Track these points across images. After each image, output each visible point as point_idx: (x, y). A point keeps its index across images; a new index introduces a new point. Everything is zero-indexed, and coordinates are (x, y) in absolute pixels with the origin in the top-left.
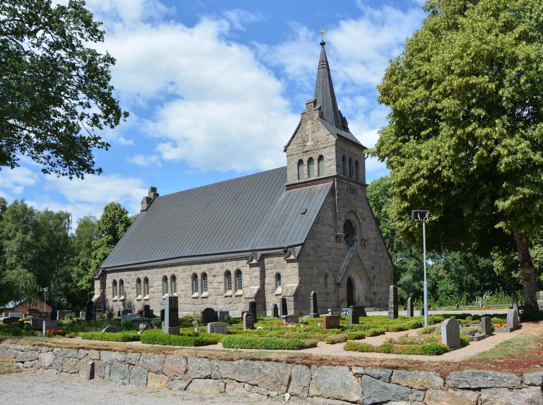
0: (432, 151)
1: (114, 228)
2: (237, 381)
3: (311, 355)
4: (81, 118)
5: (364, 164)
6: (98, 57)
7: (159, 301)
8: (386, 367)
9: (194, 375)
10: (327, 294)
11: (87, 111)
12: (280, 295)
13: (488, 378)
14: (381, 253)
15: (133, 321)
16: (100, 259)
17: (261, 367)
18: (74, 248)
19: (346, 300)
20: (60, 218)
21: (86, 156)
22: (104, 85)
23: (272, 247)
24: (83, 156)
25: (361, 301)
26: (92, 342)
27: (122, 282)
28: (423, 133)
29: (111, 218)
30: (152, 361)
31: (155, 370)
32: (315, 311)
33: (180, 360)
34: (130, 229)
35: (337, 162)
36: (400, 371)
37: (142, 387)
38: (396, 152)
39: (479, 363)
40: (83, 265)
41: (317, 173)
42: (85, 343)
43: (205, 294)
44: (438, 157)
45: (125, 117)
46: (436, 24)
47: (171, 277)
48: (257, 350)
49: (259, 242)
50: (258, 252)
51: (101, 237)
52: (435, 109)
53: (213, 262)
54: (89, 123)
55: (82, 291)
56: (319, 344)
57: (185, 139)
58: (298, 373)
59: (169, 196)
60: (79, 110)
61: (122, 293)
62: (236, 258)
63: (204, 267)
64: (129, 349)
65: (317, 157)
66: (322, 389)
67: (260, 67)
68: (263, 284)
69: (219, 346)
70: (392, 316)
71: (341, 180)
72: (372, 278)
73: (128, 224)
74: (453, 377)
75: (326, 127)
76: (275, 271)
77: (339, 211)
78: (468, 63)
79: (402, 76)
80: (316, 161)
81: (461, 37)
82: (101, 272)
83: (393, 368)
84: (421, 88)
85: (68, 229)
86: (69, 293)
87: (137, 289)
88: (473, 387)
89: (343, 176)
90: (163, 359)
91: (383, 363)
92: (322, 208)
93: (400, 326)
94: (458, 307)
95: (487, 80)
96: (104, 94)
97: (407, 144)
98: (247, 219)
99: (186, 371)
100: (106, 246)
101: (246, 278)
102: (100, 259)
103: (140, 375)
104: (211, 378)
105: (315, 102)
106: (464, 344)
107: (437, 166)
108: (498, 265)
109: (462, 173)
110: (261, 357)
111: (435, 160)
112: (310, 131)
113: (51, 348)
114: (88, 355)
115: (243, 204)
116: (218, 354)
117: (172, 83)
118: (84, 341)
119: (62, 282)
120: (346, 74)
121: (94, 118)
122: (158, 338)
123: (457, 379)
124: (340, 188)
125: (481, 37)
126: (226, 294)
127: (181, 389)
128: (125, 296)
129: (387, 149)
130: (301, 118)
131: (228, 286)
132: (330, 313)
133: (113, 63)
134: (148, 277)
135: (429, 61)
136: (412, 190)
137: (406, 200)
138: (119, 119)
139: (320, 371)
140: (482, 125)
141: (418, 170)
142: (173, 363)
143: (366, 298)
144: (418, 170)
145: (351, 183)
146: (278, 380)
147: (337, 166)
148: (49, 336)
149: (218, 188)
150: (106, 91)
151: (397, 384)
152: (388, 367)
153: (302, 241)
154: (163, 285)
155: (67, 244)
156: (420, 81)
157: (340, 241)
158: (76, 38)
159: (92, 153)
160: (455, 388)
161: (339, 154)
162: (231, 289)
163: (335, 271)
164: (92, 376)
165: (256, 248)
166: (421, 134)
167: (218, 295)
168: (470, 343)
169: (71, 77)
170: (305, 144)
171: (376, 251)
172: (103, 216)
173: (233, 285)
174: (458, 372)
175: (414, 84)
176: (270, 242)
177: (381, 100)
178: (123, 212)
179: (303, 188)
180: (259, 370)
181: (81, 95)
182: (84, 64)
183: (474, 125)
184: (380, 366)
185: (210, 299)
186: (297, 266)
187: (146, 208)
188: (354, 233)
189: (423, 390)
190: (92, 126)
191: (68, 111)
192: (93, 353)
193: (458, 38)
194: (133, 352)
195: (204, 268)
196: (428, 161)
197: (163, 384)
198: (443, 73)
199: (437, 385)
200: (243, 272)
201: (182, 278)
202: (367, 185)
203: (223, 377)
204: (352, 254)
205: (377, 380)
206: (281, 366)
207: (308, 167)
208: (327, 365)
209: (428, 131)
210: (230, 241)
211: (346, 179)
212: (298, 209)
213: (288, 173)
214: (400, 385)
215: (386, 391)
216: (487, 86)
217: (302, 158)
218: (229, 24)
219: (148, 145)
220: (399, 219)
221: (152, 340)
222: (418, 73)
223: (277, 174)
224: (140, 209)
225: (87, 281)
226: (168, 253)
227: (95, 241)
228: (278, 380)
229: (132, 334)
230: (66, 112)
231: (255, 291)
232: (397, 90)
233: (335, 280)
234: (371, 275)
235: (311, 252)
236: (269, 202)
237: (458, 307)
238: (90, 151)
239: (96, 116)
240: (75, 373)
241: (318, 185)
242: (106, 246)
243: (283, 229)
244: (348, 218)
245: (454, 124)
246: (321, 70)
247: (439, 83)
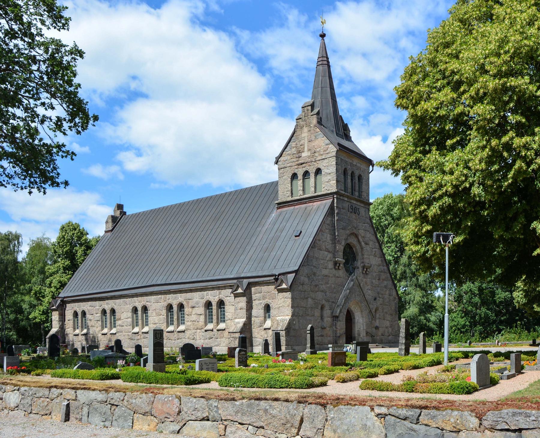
0: (457, 165)
1: (71, 251)
2: (240, 423)
3: (325, 395)
4: (42, 122)
5: (369, 179)
6: (63, 48)
7: (128, 335)
8: (413, 407)
9: (188, 416)
10: (323, 328)
11: (49, 113)
12: (269, 329)
13: (531, 418)
14: (385, 282)
15: (106, 357)
16: (55, 287)
17: (268, 407)
18: (25, 274)
19: (345, 335)
20: (8, 239)
21: (50, 167)
22: (70, 83)
23: (260, 274)
24: (46, 166)
25: (361, 336)
26: (64, 380)
27: (84, 313)
28: (449, 142)
29: (68, 240)
30: (138, 401)
31: (143, 411)
32: (312, 346)
33: (172, 400)
34: (93, 254)
35: (338, 176)
36: (430, 411)
37: (127, 430)
38: (416, 164)
39: (515, 402)
40: (35, 294)
41: (313, 189)
42: (57, 381)
43: (182, 328)
44: (465, 172)
45: (94, 122)
46: (465, 13)
47: (142, 308)
48: (260, 389)
49: (246, 269)
50: (245, 280)
51: (55, 262)
52: (462, 114)
53: (191, 291)
54: (51, 127)
55: (36, 324)
56: (330, 382)
57: (151, 147)
58: (311, 414)
59: (138, 215)
60: (41, 111)
61: (85, 325)
62: (219, 287)
63: (181, 297)
64: (110, 388)
65: (314, 171)
66: (339, 431)
67: (240, 59)
68: (249, 317)
69: (214, 385)
70: (403, 353)
71: (341, 198)
72: (374, 310)
73: (88, 247)
74: (490, 418)
75: (325, 135)
76: (264, 302)
77: (338, 233)
78: (506, 62)
79: (424, 75)
80: (312, 176)
81: (498, 30)
82: (59, 301)
83: (421, 408)
84: (447, 90)
85: (18, 252)
86: (18, 326)
87: (102, 322)
88: (513, 428)
89: (343, 192)
90: (152, 399)
91: (410, 403)
92: (320, 230)
93: (415, 363)
94: (470, 343)
95: (528, 81)
96: (70, 93)
97: (428, 156)
98: (231, 242)
99: (180, 412)
100: (63, 273)
101: (229, 310)
102: (55, 287)
103: (125, 417)
104: (208, 420)
105: (312, 106)
106: (493, 383)
107: (463, 182)
108: (519, 296)
109: (495, 189)
110: (268, 397)
111: (461, 175)
112: (306, 139)
113: (17, 387)
114: (61, 394)
115: (227, 225)
116: (216, 393)
117: (134, 78)
118: (55, 379)
119: (11, 313)
120: (343, 68)
121: (57, 121)
122: (142, 376)
123: (495, 419)
124: (340, 206)
125: (521, 30)
126: (206, 328)
127: (173, 432)
128: (88, 329)
129: (404, 161)
130: (295, 124)
131: (209, 319)
132: (331, 349)
133: (81, 56)
134: (115, 308)
135: (457, 57)
136: (434, 211)
137: (428, 222)
138: (87, 123)
139: (337, 411)
140: (520, 135)
141: (440, 186)
142: (164, 403)
143: (367, 333)
144: (440, 186)
145: (352, 201)
146: (288, 422)
147: (337, 181)
148: (12, 373)
149: (196, 205)
150: (72, 89)
151: (426, 425)
152: (416, 407)
153: (296, 268)
154: (133, 317)
155: (16, 270)
156: (445, 81)
157: (339, 269)
158: (35, 25)
159: (57, 162)
160: (492, 429)
161: (340, 166)
162: (212, 322)
163: (333, 302)
164: (67, 418)
165: (242, 276)
166: (447, 144)
167: (197, 329)
168: (501, 381)
169: (31, 72)
170: (300, 154)
171: (379, 279)
172: (59, 238)
173: (215, 318)
174: (497, 412)
175: (439, 84)
176: (258, 269)
177: (399, 103)
178: (83, 233)
179: (296, 207)
180: (266, 411)
181: (44, 96)
182: (46, 56)
183: (511, 134)
184: (407, 406)
185: (188, 333)
186: (290, 296)
187: (111, 229)
188: (354, 259)
189: (455, 432)
190: (55, 131)
191: (28, 113)
192: (68, 393)
193: (494, 31)
194: (115, 392)
195: (180, 298)
196: (453, 177)
197: (152, 426)
198: (474, 73)
199: (471, 426)
200: (226, 303)
201: (155, 310)
202: (371, 204)
203: (223, 418)
204: (352, 283)
205: (403, 421)
206: (291, 406)
207: (303, 182)
208: (345, 405)
209: (455, 140)
210: (211, 267)
211: (348, 197)
212: (291, 231)
213: (279, 189)
214: (429, 426)
215: (413, 433)
216: (527, 88)
217: (296, 171)
218: (204, 5)
219: (108, 153)
220: (415, 242)
221: (135, 379)
222: (443, 72)
223: (266, 190)
224: (104, 229)
225: (41, 313)
226: (137, 281)
227: (49, 267)
228: (288, 422)
229: (109, 371)
230: (26, 114)
231: (241, 325)
232: (419, 92)
233: (332, 313)
234: (373, 306)
235: (306, 280)
236: (258, 222)
237: (470, 343)
238: (55, 160)
239: (59, 119)
240: (46, 415)
241: (315, 203)
242: (63, 273)
243: (273, 253)
244: (348, 242)
245: (487, 133)
246: (321, 67)
247: (470, 85)
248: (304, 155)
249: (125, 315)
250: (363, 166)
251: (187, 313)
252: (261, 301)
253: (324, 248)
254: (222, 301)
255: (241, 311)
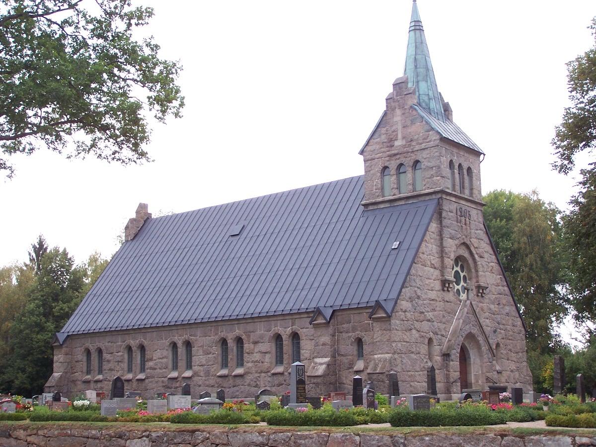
7: (163, 382)
43: (240, 371)
65: (411, 164)
101: (307, 347)
134: (145, 343)
185: (248, 378)
211: (455, 196)
248: (397, 143)
249: (159, 354)
250: (472, 158)
251: (248, 351)
252: (350, 334)
253: (429, 263)
254: (297, 333)
255: (324, 347)
